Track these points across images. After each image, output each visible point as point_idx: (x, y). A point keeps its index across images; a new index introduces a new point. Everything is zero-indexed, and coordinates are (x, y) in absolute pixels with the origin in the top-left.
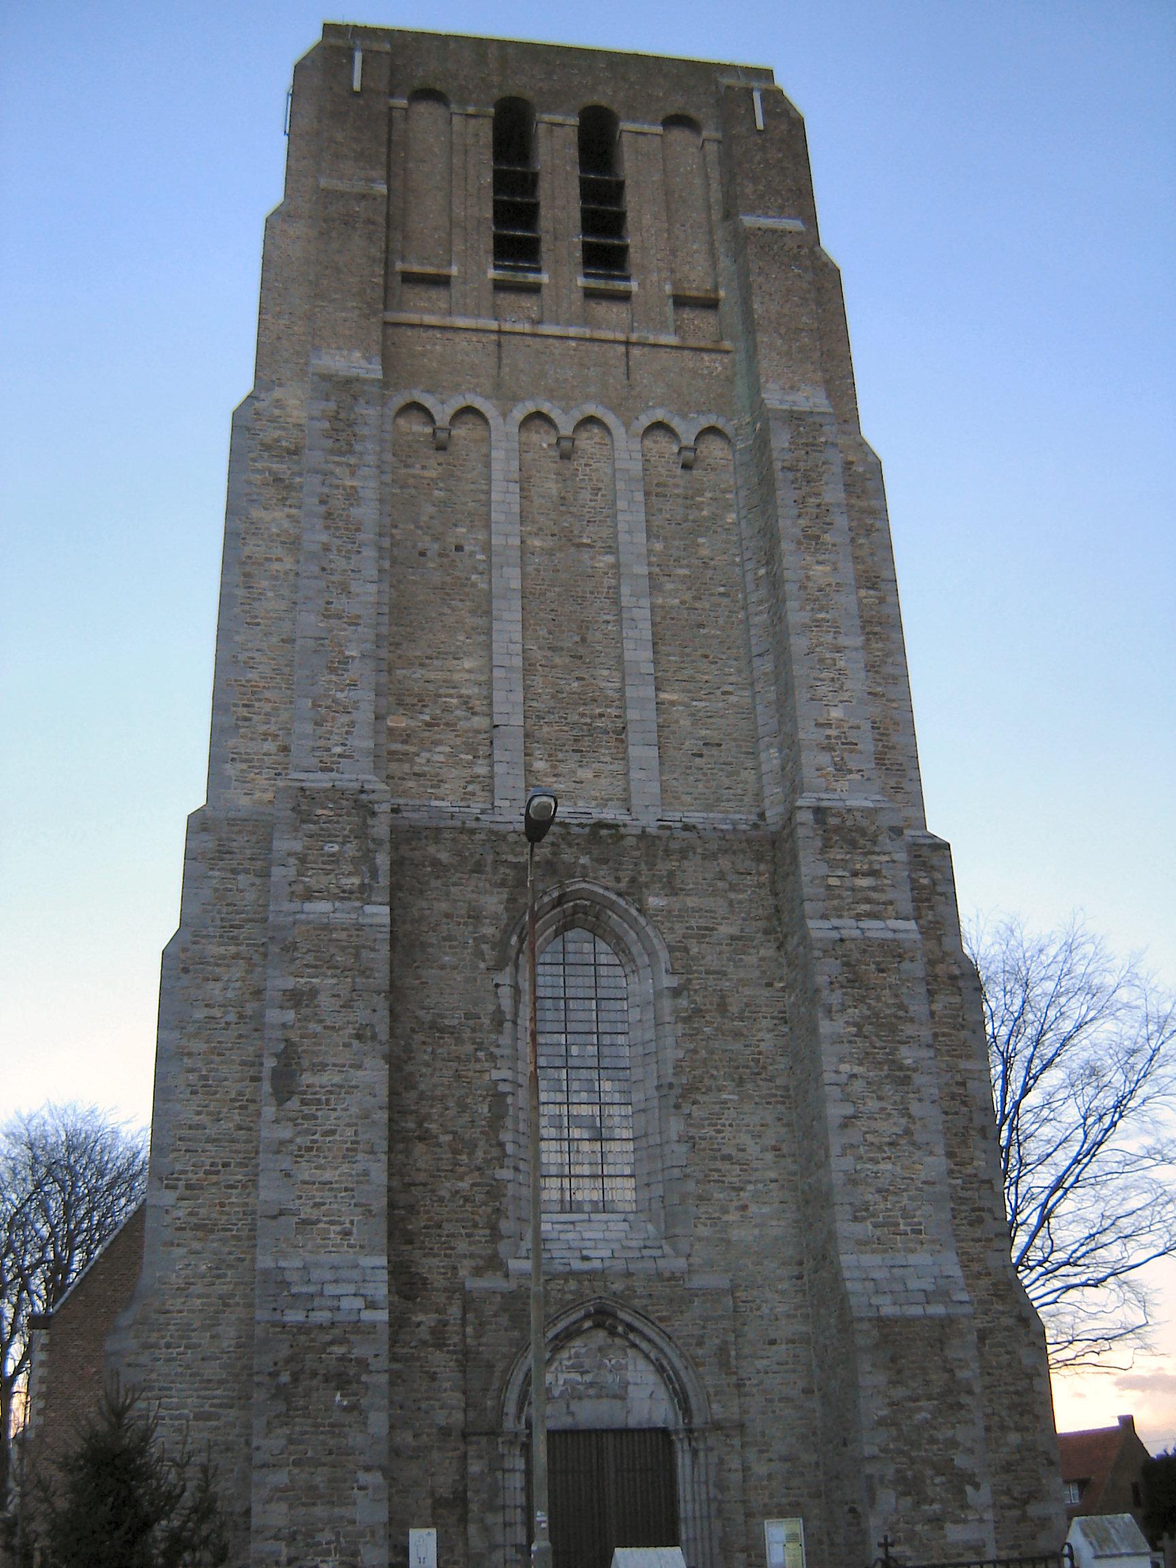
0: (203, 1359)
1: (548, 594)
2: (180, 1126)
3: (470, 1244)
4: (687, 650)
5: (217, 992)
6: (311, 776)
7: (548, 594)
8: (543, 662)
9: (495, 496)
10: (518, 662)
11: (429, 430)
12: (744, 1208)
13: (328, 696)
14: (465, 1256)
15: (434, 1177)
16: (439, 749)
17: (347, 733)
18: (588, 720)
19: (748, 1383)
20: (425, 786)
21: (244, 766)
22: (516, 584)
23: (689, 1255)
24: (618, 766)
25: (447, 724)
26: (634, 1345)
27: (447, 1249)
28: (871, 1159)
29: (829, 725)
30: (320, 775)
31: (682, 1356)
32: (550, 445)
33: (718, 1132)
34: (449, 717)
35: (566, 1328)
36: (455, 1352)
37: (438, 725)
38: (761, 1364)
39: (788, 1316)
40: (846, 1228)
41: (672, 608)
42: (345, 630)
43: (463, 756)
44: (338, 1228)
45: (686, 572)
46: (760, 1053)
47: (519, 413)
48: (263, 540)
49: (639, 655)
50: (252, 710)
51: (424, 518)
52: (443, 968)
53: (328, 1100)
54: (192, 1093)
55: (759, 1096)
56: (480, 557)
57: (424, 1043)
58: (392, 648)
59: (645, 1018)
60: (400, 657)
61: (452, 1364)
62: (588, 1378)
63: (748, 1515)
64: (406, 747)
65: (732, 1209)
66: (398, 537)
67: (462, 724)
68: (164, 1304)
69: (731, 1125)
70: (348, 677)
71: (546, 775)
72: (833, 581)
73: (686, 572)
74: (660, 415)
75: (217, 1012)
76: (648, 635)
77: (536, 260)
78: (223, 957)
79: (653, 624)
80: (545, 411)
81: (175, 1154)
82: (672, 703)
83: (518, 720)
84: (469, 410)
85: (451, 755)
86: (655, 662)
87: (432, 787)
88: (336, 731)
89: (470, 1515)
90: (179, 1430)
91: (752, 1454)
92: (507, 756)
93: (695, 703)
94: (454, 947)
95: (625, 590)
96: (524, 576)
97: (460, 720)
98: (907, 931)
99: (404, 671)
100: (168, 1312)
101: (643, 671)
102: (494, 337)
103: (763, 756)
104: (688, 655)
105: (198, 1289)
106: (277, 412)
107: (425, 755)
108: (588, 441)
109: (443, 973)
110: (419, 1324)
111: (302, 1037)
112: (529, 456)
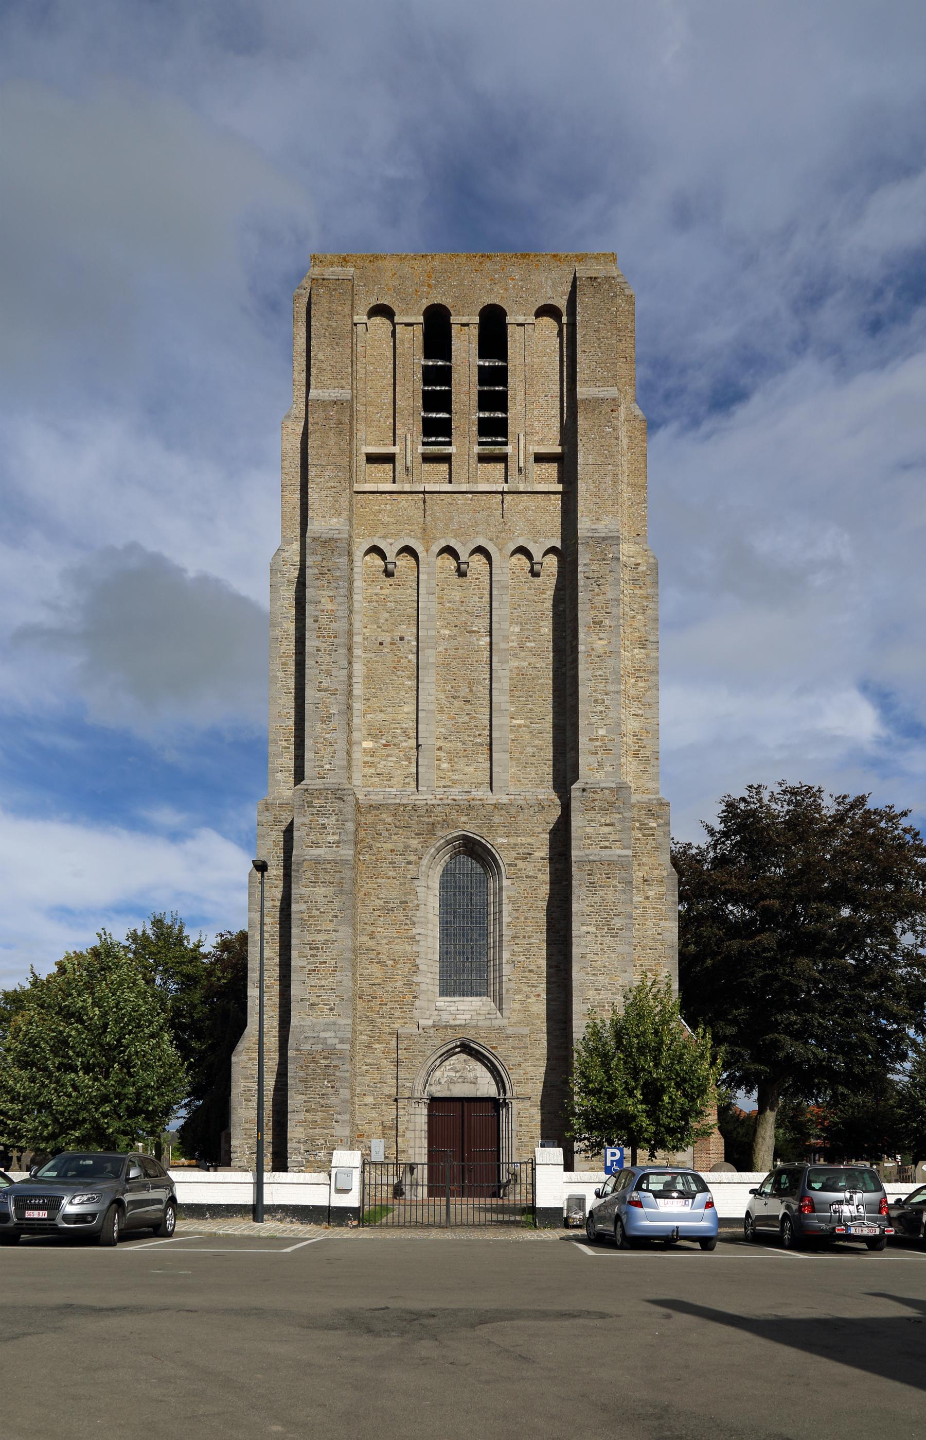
3: (401, 1012)
14: (399, 1018)
16: (390, 759)
17: (332, 757)
18: (472, 739)
28: (594, 974)
29: (597, 740)
33: (527, 958)
34: (396, 740)
36: (393, 1062)
37: (390, 746)
40: (265, 1069)
42: (329, 698)
43: (403, 763)
44: (328, 1007)
45: (533, 644)
47: (436, 549)
52: (389, 878)
53: (322, 948)
60: (369, 707)
62: (458, 1075)
64: (373, 759)
65: (532, 996)
67: (404, 744)
70: (332, 725)
71: (448, 771)
72: (608, 650)
73: (533, 644)
74: (521, 542)
82: (520, 726)
88: (325, 756)
93: (533, 725)
94: (395, 867)
97: (402, 742)
98: (626, 856)
102: (421, 496)
104: (531, 696)
107: (383, 763)
109: (389, 880)
110: (376, 1049)
111: (309, 917)
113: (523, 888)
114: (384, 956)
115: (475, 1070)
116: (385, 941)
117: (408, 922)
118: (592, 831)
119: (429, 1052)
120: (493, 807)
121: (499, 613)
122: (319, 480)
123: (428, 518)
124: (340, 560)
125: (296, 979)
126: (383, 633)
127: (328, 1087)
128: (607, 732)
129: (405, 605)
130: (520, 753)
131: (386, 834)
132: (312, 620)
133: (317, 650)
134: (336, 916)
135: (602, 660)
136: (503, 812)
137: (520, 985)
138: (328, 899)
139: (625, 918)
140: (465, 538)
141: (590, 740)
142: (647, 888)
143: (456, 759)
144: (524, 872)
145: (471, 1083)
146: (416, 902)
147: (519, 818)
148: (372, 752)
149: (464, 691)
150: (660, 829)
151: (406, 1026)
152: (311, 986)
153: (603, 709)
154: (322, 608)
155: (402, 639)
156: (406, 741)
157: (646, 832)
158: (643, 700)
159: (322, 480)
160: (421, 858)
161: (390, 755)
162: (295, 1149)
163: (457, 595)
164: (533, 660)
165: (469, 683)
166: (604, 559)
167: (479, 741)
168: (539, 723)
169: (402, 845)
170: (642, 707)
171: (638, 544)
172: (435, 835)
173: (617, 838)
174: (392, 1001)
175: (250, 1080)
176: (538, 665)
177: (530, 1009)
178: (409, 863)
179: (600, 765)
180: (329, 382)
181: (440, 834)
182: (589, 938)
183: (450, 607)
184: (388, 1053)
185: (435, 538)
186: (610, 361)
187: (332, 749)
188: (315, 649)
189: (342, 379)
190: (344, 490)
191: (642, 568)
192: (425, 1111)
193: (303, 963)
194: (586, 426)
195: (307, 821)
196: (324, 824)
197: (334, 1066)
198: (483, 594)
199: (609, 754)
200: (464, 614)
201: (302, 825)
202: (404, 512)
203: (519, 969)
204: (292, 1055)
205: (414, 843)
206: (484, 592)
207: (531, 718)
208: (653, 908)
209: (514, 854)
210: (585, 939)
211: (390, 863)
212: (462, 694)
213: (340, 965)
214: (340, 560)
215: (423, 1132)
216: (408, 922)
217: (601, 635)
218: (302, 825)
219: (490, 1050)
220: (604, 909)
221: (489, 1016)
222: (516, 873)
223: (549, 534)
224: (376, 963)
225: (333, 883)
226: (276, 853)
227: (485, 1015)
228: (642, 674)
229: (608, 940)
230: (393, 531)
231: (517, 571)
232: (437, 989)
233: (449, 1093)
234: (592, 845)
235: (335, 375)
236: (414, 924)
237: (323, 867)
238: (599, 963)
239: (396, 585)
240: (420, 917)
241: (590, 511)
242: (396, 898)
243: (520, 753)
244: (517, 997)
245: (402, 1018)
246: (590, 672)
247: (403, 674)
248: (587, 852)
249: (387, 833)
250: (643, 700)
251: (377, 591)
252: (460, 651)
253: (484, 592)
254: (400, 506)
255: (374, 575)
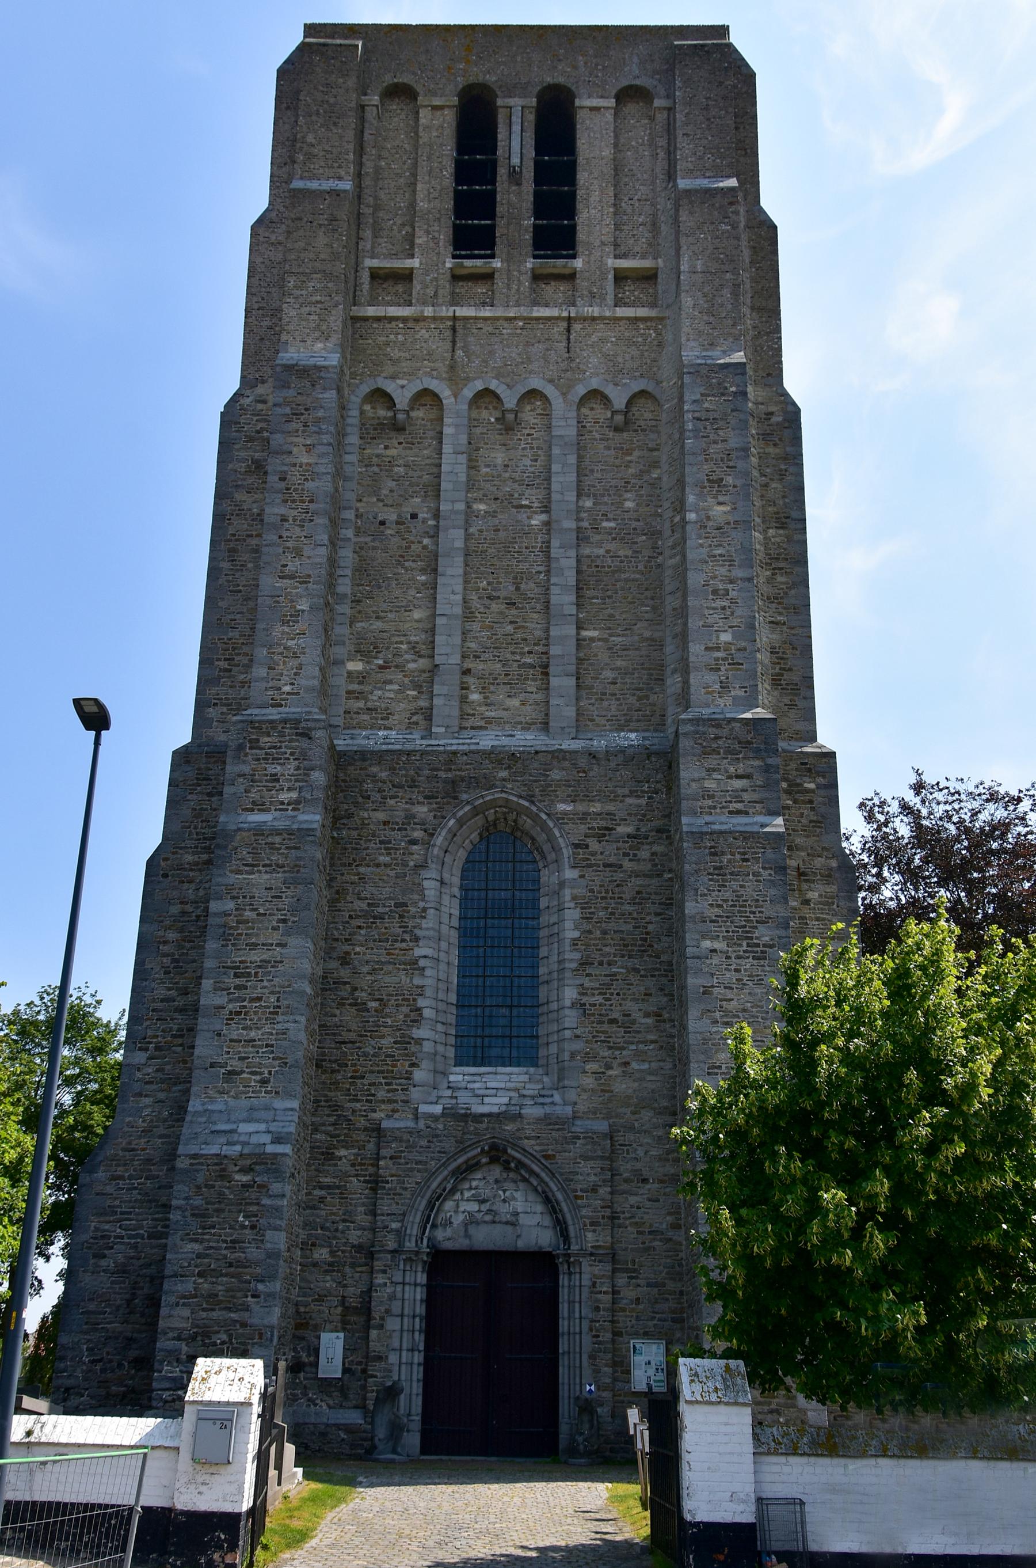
0: (159, 1188)
1: (490, 550)
2: (154, 1001)
3: (388, 1091)
4: (609, 593)
5: (190, 891)
6: (264, 711)
7: (490, 550)
8: (481, 610)
9: (444, 468)
10: (458, 610)
11: (390, 414)
12: (626, 1064)
13: (280, 645)
14: (383, 1102)
15: (361, 1036)
17: (296, 674)
18: (518, 658)
19: (622, 1216)
20: (376, 719)
21: (225, 709)
22: (459, 544)
23: (576, 1103)
24: (539, 696)
25: (397, 667)
26: (525, 1180)
27: (368, 1095)
30: (274, 711)
31: (563, 1189)
32: (497, 419)
34: (399, 660)
35: (466, 1162)
38: (633, 1200)
39: (660, 1159)
41: (598, 557)
42: (296, 588)
43: (408, 692)
44: (258, 1078)
45: (612, 524)
46: (647, 933)
47: (468, 393)
48: (246, 519)
49: (563, 599)
50: (232, 663)
51: (384, 492)
52: (378, 865)
53: (256, 973)
54: (165, 973)
55: (645, 970)
56: (431, 522)
57: (359, 927)
58: (354, 604)
59: (551, 905)
60: (360, 612)
61: (367, 1191)
62: (485, 1207)
63: (617, 1334)
64: (362, 687)
65: (615, 1065)
66: (361, 510)
67: (412, 666)
68: (130, 1143)
69: (618, 994)
70: (298, 628)
71: (480, 705)
72: (731, 519)
73: (612, 524)
74: (595, 383)
75: (189, 908)
76: (572, 581)
77: (492, 248)
78: (197, 864)
79: (578, 572)
80: (492, 387)
81: (148, 1023)
82: (592, 639)
83: (456, 659)
84: (426, 392)
85: (399, 692)
86: (578, 605)
87: (382, 719)
88: (285, 672)
89: (373, 1322)
90: (135, 1247)
91: (621, 1280)
92: (444, 690)
93: (613, 639)
95: (555, 543)
96: (468, 537)
97: (408, 662)
99: (363, 624)
100: (133, 1150)
101: (566, 612)
103: (669, 681)
104: (609, 597)
105: (162, 1131)
106: (260, 406)
108: (530, 416)
109: (378, 870)
110: (340, 1159)
111: (238, 922)
112: (478, 431)
113: (598, 883)
114: (363, 994)
115: (514, 1199)
116: (365, 969)
117: (407, 937)
118: (714, 786)
119: (433, 1163)
120: (550, 756)
121: (561, 479)
122: (299, 292)
123: (459, 353)
124: (325, 396)
125: (205, 1027)
126: (386, 509)
127: (243, 1227)
128: (735, 636)
129: (421, 470)
130: (592, 678)
131: (377, 797)
132: (276, 478)
133: (282, 520)
134: (284, 921)
135: (722, 533)
136: (567, 764)
137: (595, 1046)
138: (273, 893)
139: (777, 927)
140: (512, 379)
141: (707, 649)
142: (805, 886)
143: (492, 688)
144: (600, 857)
145: (507, 1223)
146: (421, 904)
147: (591, 774)
148: (361, 678)
149: (507, 589)
150: (822, 792)
151: (396, 1115)
152: (231, 1040)
153: (726, 603)
154: (294, 461)
155: (414, 516)
156: (415, 661)
157: (801, 797)
158: (785, 601)
159: (304, 292)
160: (432, 835)
161: (390, 682)
162: (170, 1352)
163: (499, 457)
164: (612, 546)
165: (516, 578)
166: (723, 395)
167: (529, 661)
168: (623, 635)
169: (402, 814)
170: (784, 611)
171: (770, 386)
172: (456, 798)
173: (755, 796)
174: (372, 1072)
175: (107, 1218)
176: (621, 553)
177: (613, 1088)
178: (414, 842)
179: (725, 687)
180: (321, 171)
181: (465, 797)
182: (715, 961)
183: (487, 473)
184: (361, 1164)
185: (468, 379)
186: (726, 145)
187: (296, 662)
188: (279, 518)
189: (340, 167)
190: (336, 306)
191: (776, 419)
192: (422, 1278)
193: (220, 999)
194: (691, 224)
195: (246, 769)
196: (276, 775)
197: (259, 1186)
198: (539, 456)
199: (740, 669)
200: (509, 483)
201: (239, 776)
202: (423, 344)
203: (592, 1018)
204: (182, 1166)
205: (422, 810)
206: (540, 452)
207: (610, 628)
208: (818, 919)
209: (583, 828)
210: (708, 961)
211: (381, 842)
212: (503, 594)
213: (286, 1002)
214: (325, 396)
215: (417, 1320)
216: (407, 937)
217: (721, 499)
218: (239, 776)
219: (543, 1161)
220: (739, 911)
221: (541, 1100)
222: (588, 859)
223: (636, 374)
224: (350, 1005)
225: (283, 866)
226: (196, 828)
227: (533, 1097)
228: (781, 565)
229: (748, 963)
230: (405, 370)
231: (588, 425)
232: (451, 1053)
233: (467, 1242)
234: (715, 808)
235: (330, 162)
236: (417, 939)
237: (270, 840)
238: (734, 1003)
239: (407, 443)
240: (427, 929)
241: (700, 333)
242: (390, 898)
243: (592, 678)
244: (592, 1067)
245: (390, 1101)
246: (705, 550)
247: (413, 565)
248: (708, 818)
249: (378, 795)
250: (785, 601)
251: (379, 451)
252: (502, 534)
253: (540, 452)
254: (417, 337)
255: (375, 429)
